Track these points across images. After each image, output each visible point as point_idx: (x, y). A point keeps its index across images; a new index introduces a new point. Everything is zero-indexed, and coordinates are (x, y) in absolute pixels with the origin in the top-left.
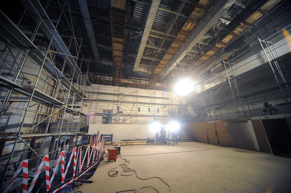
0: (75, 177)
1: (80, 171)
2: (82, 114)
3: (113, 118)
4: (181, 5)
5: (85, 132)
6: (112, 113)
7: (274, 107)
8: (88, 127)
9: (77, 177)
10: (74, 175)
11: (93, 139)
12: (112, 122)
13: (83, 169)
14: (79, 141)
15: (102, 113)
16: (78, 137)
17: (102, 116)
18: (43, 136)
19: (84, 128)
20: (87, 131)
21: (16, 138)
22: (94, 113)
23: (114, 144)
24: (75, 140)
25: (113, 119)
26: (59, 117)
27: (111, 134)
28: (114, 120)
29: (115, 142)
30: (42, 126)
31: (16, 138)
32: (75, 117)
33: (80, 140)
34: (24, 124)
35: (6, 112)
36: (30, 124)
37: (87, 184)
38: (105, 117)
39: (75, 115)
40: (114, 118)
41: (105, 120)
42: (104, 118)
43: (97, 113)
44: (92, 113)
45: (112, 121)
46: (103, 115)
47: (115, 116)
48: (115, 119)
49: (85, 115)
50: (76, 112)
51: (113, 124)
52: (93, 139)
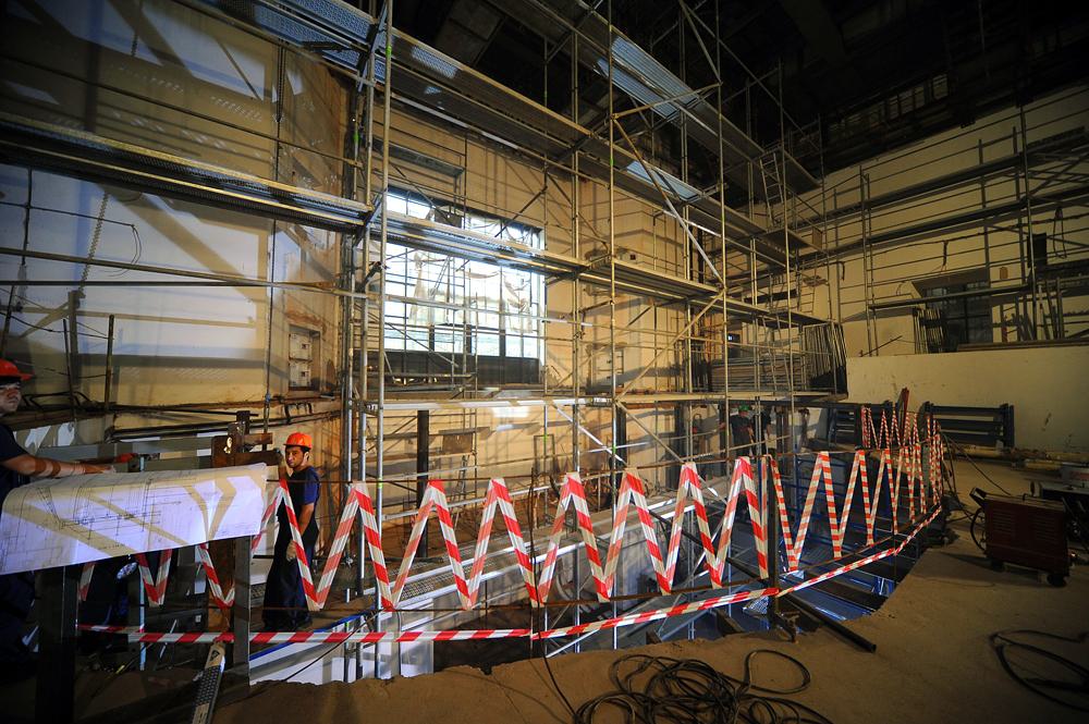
4: (697, 417)
8: (842, 373)
14: (813, 427)
17: (915, 315)
20: (843, 389)
22: (862, 308)
23: (1028, 464)
37: (844, 645)
40: (1009, 316)
41: (937, 334)
43: (878, 302)
48: (1019, 321)
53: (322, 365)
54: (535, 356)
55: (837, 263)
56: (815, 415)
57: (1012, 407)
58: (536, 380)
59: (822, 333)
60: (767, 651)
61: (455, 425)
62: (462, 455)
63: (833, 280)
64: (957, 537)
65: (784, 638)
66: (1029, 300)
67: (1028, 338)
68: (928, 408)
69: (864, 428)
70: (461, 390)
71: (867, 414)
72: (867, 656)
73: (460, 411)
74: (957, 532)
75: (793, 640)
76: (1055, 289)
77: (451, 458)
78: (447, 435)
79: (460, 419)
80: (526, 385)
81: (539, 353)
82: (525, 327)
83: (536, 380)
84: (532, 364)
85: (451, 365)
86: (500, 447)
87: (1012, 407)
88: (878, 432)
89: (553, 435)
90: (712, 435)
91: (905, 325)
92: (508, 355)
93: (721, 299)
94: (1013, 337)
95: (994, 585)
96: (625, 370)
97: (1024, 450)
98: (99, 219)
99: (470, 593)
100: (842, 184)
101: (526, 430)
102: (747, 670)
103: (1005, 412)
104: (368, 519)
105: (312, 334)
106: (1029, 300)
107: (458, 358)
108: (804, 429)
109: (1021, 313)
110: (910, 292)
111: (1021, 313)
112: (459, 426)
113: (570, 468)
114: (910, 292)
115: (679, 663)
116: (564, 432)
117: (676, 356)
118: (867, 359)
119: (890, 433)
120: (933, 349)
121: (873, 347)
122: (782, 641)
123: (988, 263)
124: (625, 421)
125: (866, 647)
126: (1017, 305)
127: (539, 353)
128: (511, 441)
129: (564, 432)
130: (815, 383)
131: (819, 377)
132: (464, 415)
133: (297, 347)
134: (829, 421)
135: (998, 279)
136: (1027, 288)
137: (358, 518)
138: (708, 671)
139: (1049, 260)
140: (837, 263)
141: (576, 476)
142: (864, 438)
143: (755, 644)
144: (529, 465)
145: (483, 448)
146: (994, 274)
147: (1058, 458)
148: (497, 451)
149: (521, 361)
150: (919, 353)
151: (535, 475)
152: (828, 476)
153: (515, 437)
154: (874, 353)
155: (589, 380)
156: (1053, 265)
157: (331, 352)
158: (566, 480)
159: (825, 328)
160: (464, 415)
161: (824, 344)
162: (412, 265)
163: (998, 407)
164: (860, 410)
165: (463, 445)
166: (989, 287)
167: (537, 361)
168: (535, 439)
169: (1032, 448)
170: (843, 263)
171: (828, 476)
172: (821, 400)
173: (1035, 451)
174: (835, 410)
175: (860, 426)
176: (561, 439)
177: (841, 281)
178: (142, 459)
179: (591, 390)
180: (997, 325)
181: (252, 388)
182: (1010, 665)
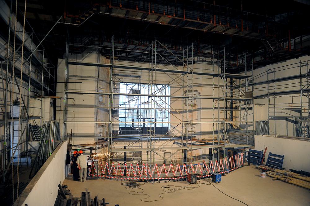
20: (253, 145)
27: (282, 155)
53: (105, 133)
55: (268, 98)
63: (267, 104)
82: (163, 117)
85: (50, 73)
89: (171, 153)
90: (85, 154)
98: (67, 98)
100: (260, 73)
103: (282, 157)
105: (103, 126)
116: (176, 152)
129: (176, 152)
133: (99, 130)
137: (107, 166)
140: (268, 98)
144: (162, 162)
152: (185, 167)
157: (107, 129)
162: (154, 74)
167: (168, 128)
168: (164, 154)
170: (269, 98)
171: (185, 167)
178: (220, 179)
181: (92, 141)
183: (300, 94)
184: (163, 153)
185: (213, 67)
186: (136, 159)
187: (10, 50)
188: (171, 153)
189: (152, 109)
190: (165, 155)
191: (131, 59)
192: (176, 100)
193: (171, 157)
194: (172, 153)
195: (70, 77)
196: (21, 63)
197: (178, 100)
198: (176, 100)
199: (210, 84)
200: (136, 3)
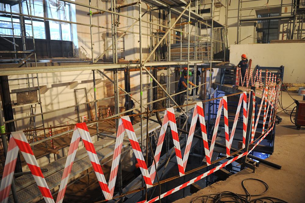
0: (245, 150)
1: (252, 140)
2: (216, 25)
3: (283, 27)
4: (162, 75)
5: (223, 61)
6: (69, 127)
7: (249, 67)
8: (228, 52)
9: (249, 150)
10: (244, 146)
11: (243, 75)
12: (280, 39)
13: (258, 135)
14: (214, 78)
15: (253, 17)
16: (212, 70)
17: (255, 26)
18: (164, 66)
19: (220, 52)
20: (228, 59)
21: (140, 68)
22: (235, 21)
23: (289, 89)
24: (208, 73)
25: (281, 30)
26: (187, 18)
27: (279, 66)
28: (283, 32)
29: (291, 85)
30: (162, 51)
31: (140, 68)
32: (203, 32)
33: (216, 75)
34: (143, 49)
35: (122, 37)
36: (146, 48)
37: (270, 169)
38: (259, 27)
39: (204, 27)
40: (285, 28)
41: (261, 35)
42: (258, 30)
43: (243, 18)
44: (231, 22)
45: (281, 35)
46: (257, 22)
47: (287, 22)
48: (288, 31)
49: (220, 25)
50: (204, 21)
51: (283, 41)
52: (243, 75)
54: (70, 40)
56: (216, 71)
57: (284, 67)
58: (72, 55)
59: (220, 31)
60: (248, 179)
61: (23, 85)
62: (30, 104)
64: (281, 119)
65: (250, 172)
66: (292, 23)
67: (290, 39)
68: (258, 67)
69: (237, 77)
70: (24, 62)
71: (239, 71)
72: (279, 171)
73: (25, 76)
74: (281, 117)
75: (254, 172)
76: (302, 18)
77: (22, 107)
78: (19, 92)
79: (25, 81)
80: (66, 58)
81: (72, 37)
83: (72, 55)
84: (68, 45)
85: (13, 45)
86: (53, 97)
87: (284, 67)
88: (243, 79)
89: (85, 89)
91: (251, 30)
92: (52, 39)
93: (188, 10)
94: (285, 38)
95: (299, 135)
96: (126, 49)
97: (287, 83)
99: (110, 190)
101: (69, 86)
102: (245, 189)
104: (30, 159)
106: (292, 23)
107: (19, 41)
108: (211, 78)
109: (289, 28)
110: (253, 15)
111: (289, 28)
112: (26, 86)
113: (167, 107)
114: (253, 15)
115: (219, 195)
117: (152, 41)
118: (236, 45)
119: (248, 79)
120: (258, 42)
121: (239, 41)
122: (250, 173)
123: (282, 5)
124: (129, 77)
125: (277, 167)
126: (288, 24)
127: (72, 37)
128: (60, 93)
130: (216, 57)
131: (217, 54)
132: (28, 79)
134: (221, 75)
135: (284, 12)
136: (292, 18)
138: (232, 195)
139: (300, 6)
141: (172, 110)
142: (237, 81)
143: (242, 177)
145: (45, 98)
146: (283, 10)
147: (296, 86)
148: (52, 100)
149: (61, 43)
150: (254, 43)
151: (77, 110)
153: (63, 91)
154: (239, 43)
155: (104, 56)
156: (301, 8)
158: (166, 113)
159: (221, 29)
160: (28, 79)
161: (220, 38)
163: (279, 67)
164: (236, 69)
165: (31, 98)
166: (281, 16)
167: (71, 43)
168: (75, 91)
169: (289, 83)
172: (218, 65)
173: (290, 84)
174: (225, 69)
175: (235, 76)
176: (89, 91)
177: (229, 6)
179: (105, 60)
180: (281, 33)
182: (57, 144)
183: (130, 66)
184: (73, 90)
185: (64, 76)
186: (19, 109)
187: (263, 133)
188: (85, 89)
189: (26, 79)
190: (77, 93)
191: (123, 63)
192: (80, 74)
193: (86, 96)
194: (87, 89)
195: (299, 29)
196: (203, 85)
197: (83, 73)
198: (80, 74)
199: (111, 68)
200: (201, 43)
